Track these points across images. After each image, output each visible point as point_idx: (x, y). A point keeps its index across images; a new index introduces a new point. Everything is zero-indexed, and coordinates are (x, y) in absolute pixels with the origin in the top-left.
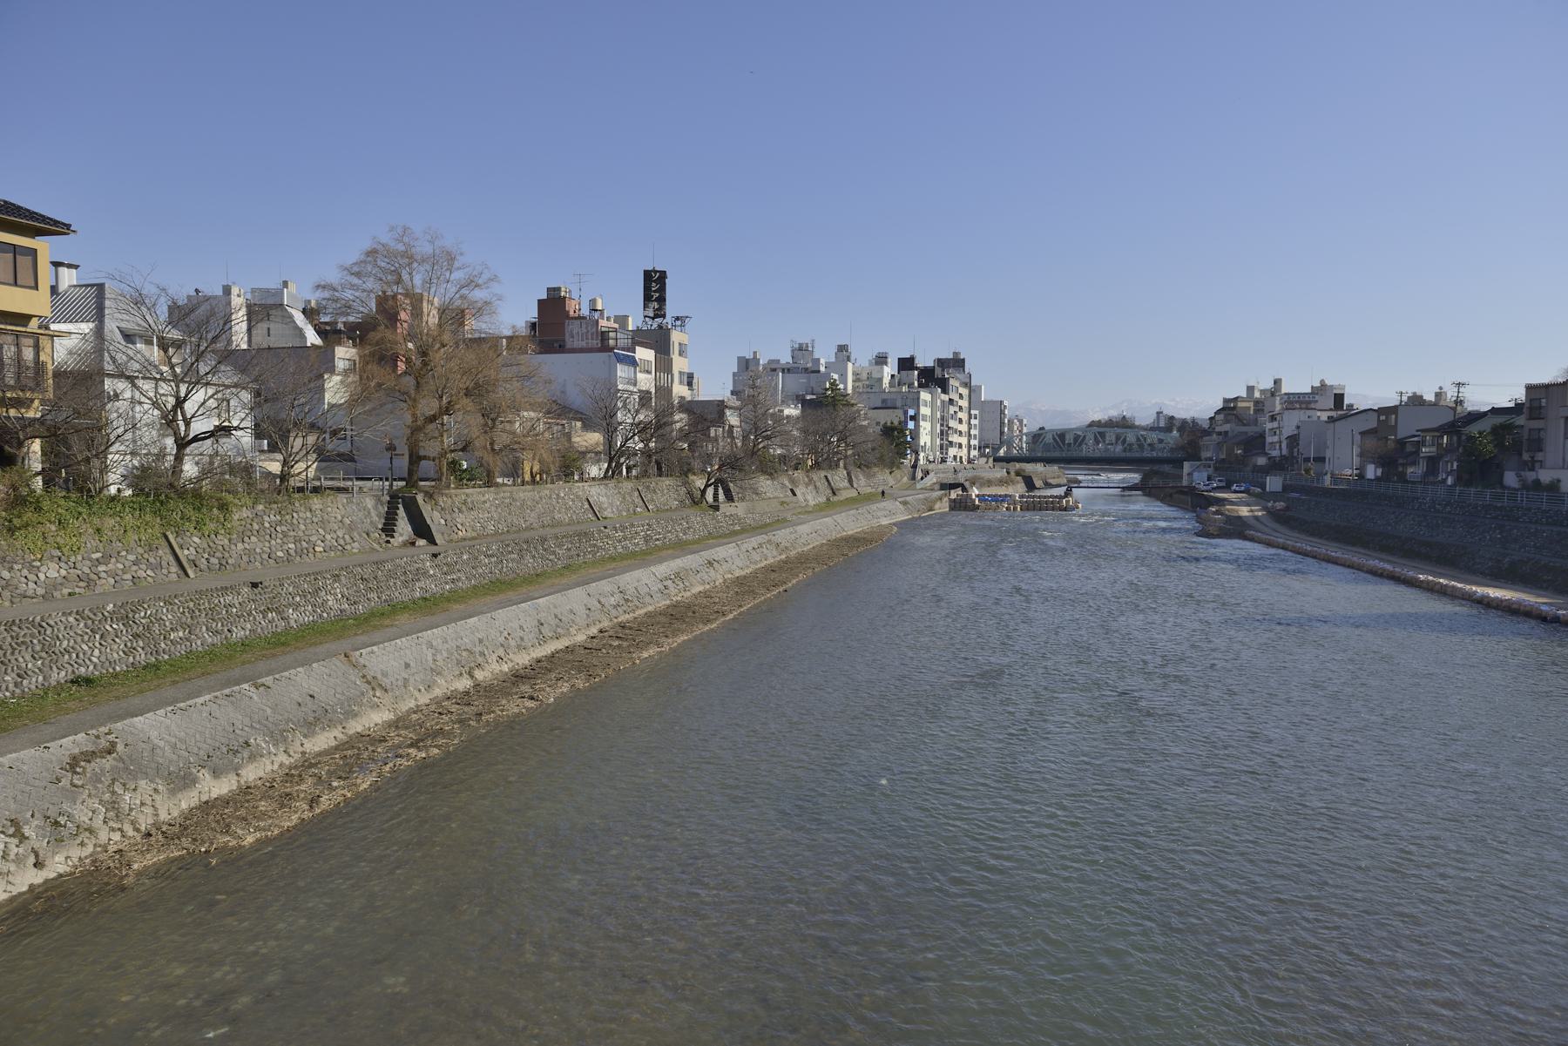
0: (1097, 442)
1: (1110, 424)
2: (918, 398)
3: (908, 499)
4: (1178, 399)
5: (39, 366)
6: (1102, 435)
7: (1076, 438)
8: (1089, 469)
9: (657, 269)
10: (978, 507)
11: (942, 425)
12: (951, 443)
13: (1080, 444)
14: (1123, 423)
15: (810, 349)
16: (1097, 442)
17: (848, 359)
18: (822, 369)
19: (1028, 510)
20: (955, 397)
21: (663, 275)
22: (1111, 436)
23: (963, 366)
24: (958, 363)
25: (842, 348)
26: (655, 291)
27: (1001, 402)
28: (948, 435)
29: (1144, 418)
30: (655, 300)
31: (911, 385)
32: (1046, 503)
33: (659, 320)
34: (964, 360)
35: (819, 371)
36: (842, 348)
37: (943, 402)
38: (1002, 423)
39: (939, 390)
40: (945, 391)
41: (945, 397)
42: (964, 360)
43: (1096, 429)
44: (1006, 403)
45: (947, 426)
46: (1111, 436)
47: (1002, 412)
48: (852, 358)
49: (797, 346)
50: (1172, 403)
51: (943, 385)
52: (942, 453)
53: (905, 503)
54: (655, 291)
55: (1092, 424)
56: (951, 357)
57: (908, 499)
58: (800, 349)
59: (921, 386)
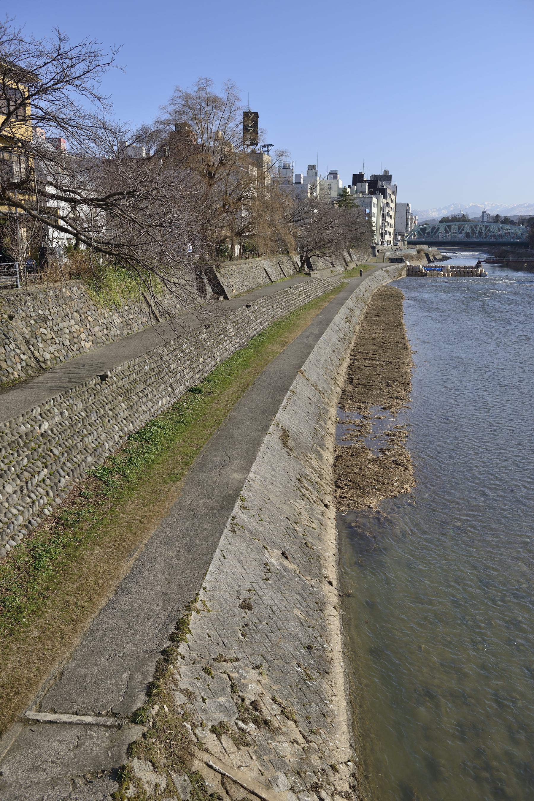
0: (447, 232)
1: (454, 219)
2: (371, 202)
3: (388, 268)
4: (486, 203)
5: (197, 144)
6: (449, 227)
7: (433, 228)
8: (445, 249)
9: (252, 111)
10: (426, 275)
11: (383, 220)
12: (386, 231)
13: (435, 233)
14: (463, 219)
15: (291, 168)
16: (447, 232)
17: (316, 174)
18: (302, 182)
19: (456, 276)
20: (389, 201)
21: (256, 114)
22: (455, 227)
23: (391, 180)
24: (387, 178)
25: (312, 167)
26: (251, 127)
27: (407, 205)
28: (385, 226)
29: (474, 214)
30: (251, 133)
31: (364, 193)
32: (468, 271)
33: (253, 147)
34: (391, 176)
35: (300, 183)
36: (312, 167)
37: (384, 204)
38: (407, 219)
39: (382, 196)
40: (385, 198)
41: (385, 201)
42: (391, 176)
43: (445, 224)
44: (410, 205)
45: (385, 221)
46: (455, 227)
47: (407, 211)
48: (319, 174)
49: (282, 166)
50: (482, 206)
51: (383, 192)
52: (382, 238)
53: (387, 271)
54: (251, 127)
55: (444, 220)
56: (382, 174)
57: (388, 268)
58: (285, 168)
59: (370, 193)
